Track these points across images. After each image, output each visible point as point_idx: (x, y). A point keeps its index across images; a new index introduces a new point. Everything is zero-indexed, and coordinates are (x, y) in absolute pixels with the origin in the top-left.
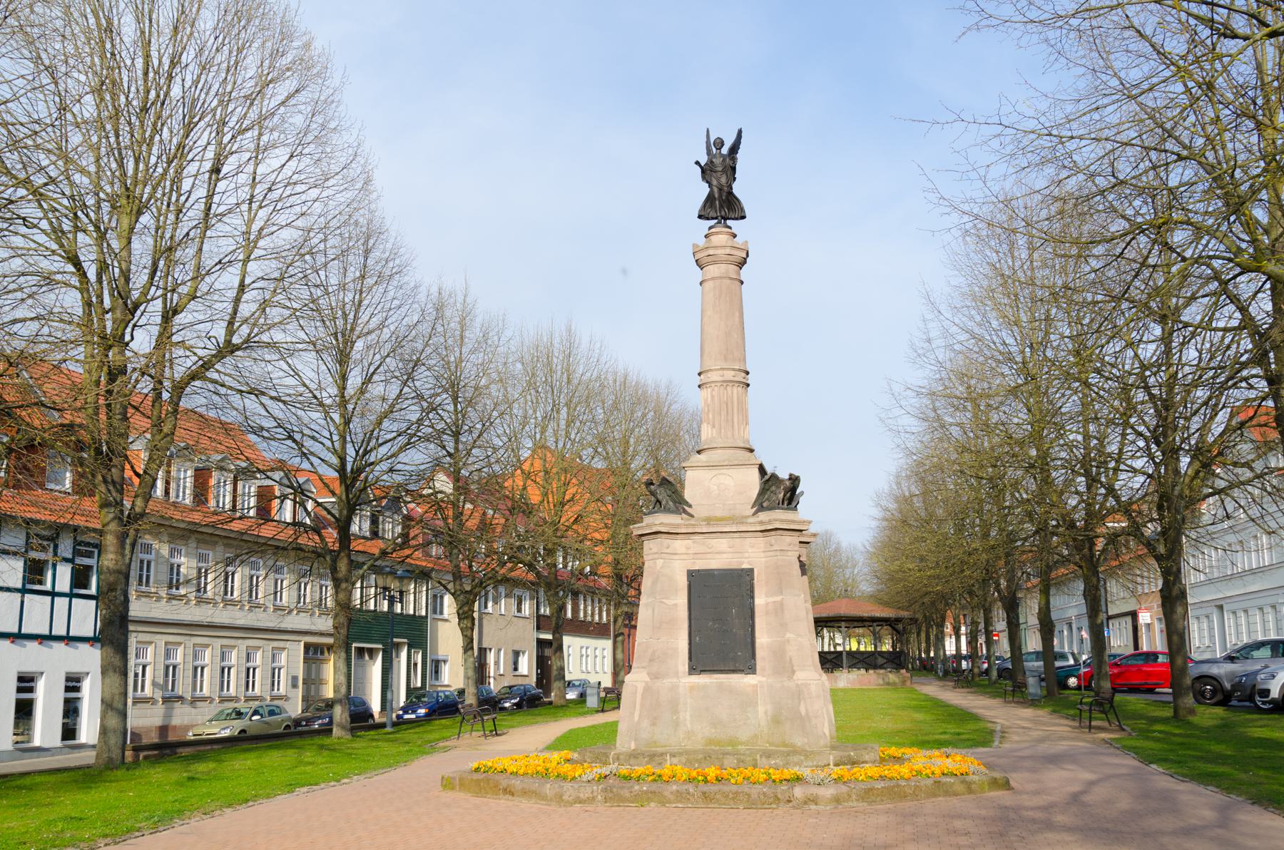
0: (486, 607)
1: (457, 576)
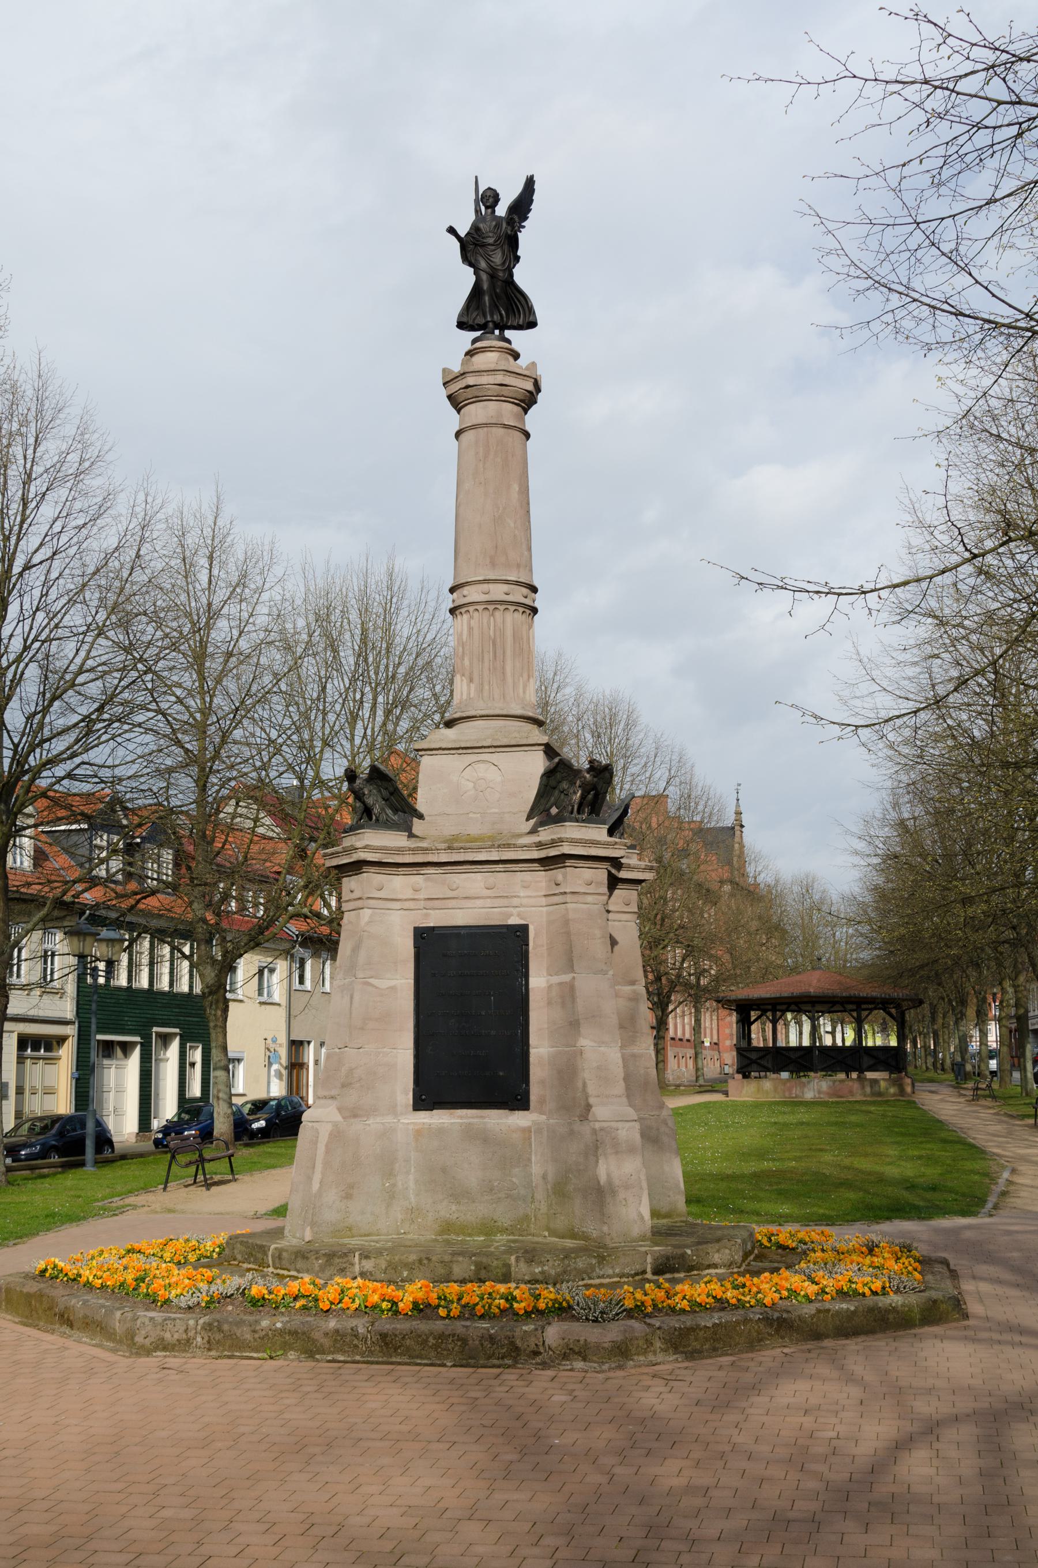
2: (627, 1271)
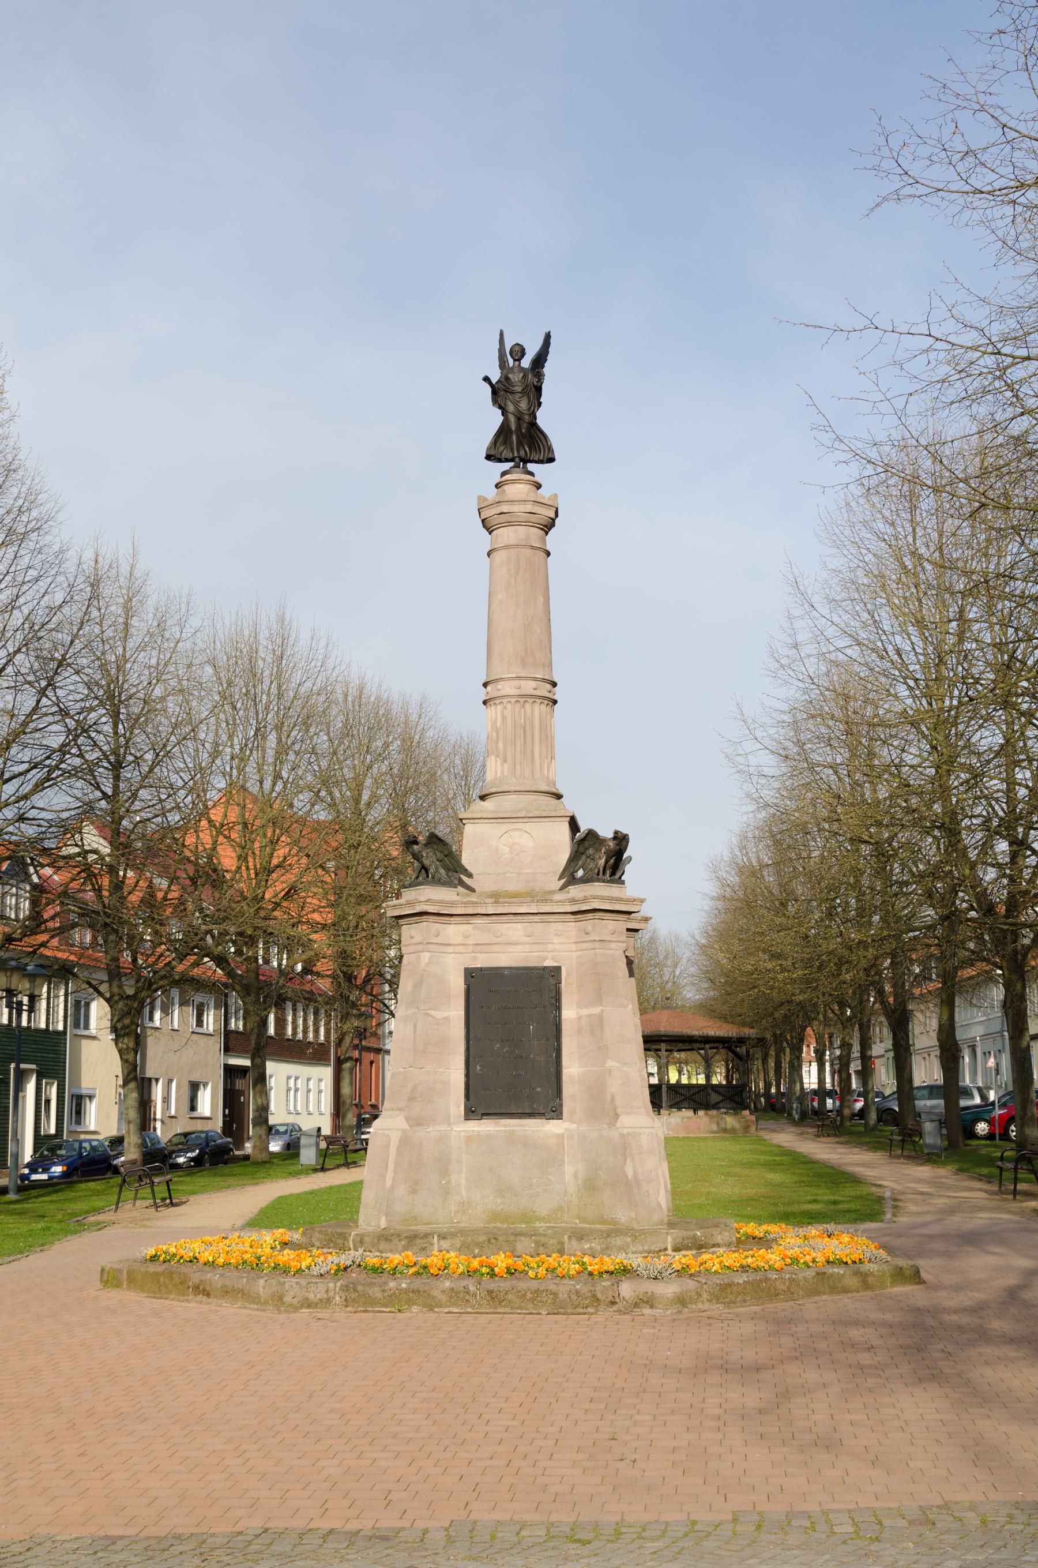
0: (151, 1019)
1: (115, 974)
2: (653, 1248)
